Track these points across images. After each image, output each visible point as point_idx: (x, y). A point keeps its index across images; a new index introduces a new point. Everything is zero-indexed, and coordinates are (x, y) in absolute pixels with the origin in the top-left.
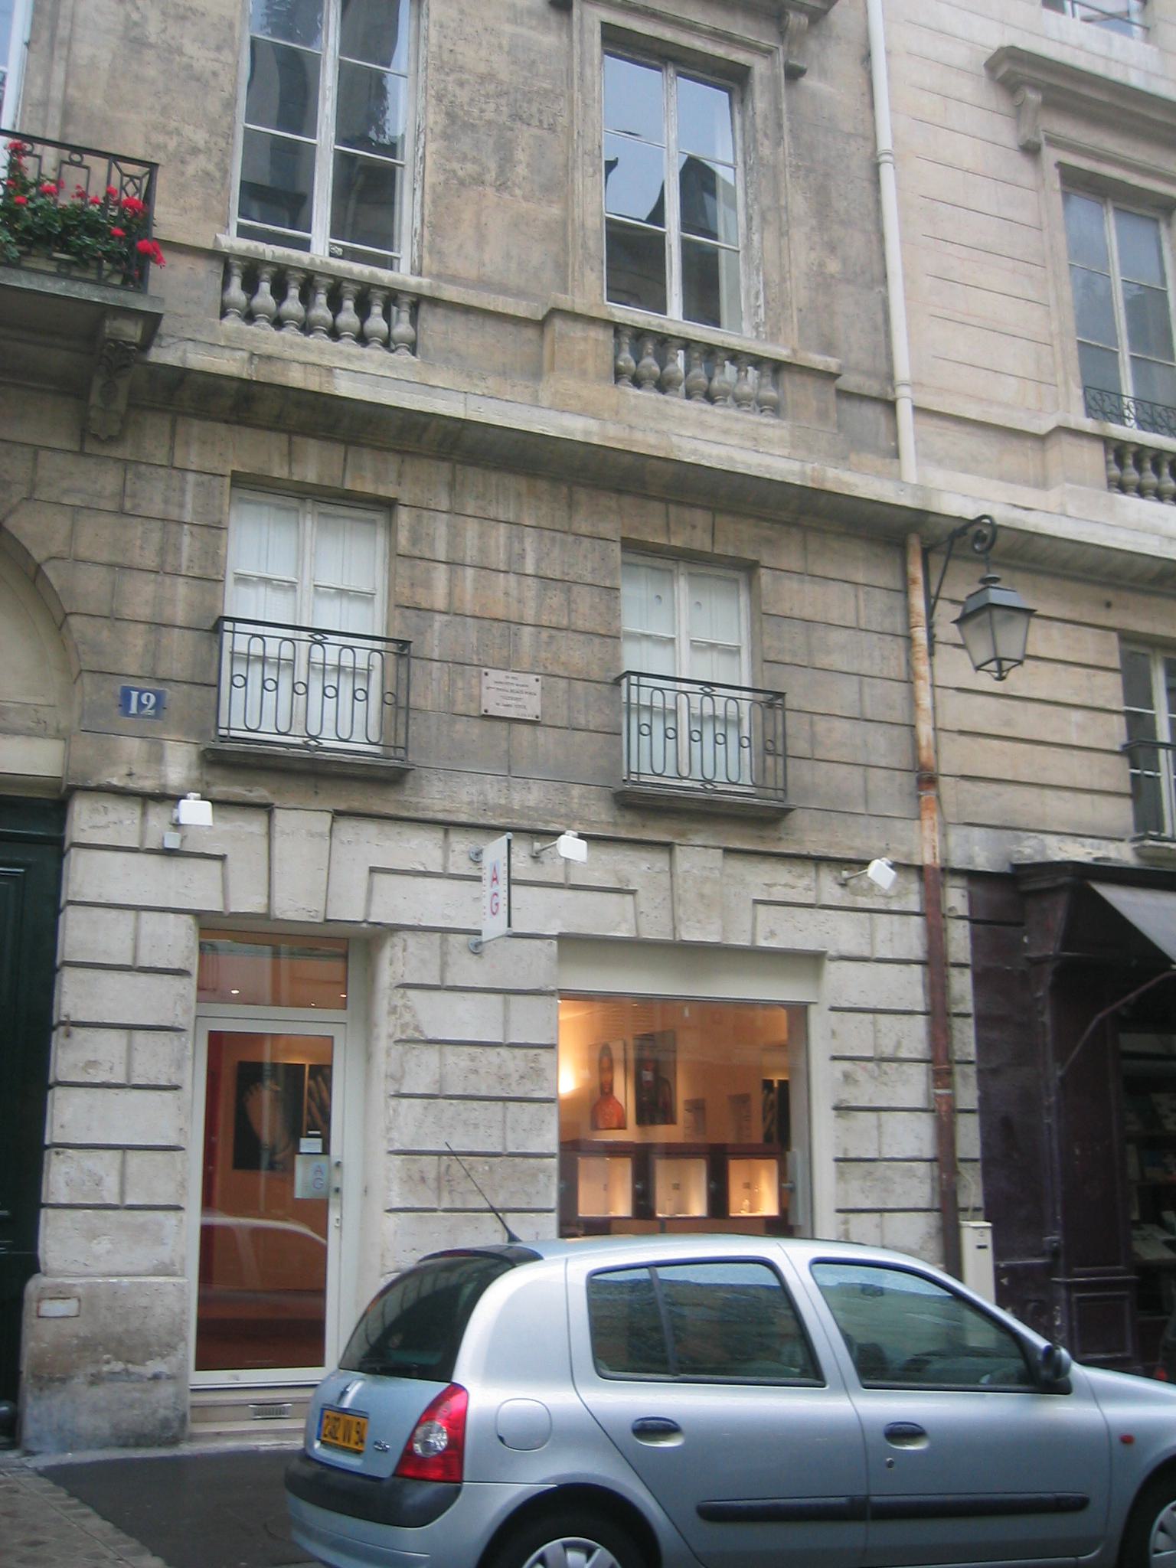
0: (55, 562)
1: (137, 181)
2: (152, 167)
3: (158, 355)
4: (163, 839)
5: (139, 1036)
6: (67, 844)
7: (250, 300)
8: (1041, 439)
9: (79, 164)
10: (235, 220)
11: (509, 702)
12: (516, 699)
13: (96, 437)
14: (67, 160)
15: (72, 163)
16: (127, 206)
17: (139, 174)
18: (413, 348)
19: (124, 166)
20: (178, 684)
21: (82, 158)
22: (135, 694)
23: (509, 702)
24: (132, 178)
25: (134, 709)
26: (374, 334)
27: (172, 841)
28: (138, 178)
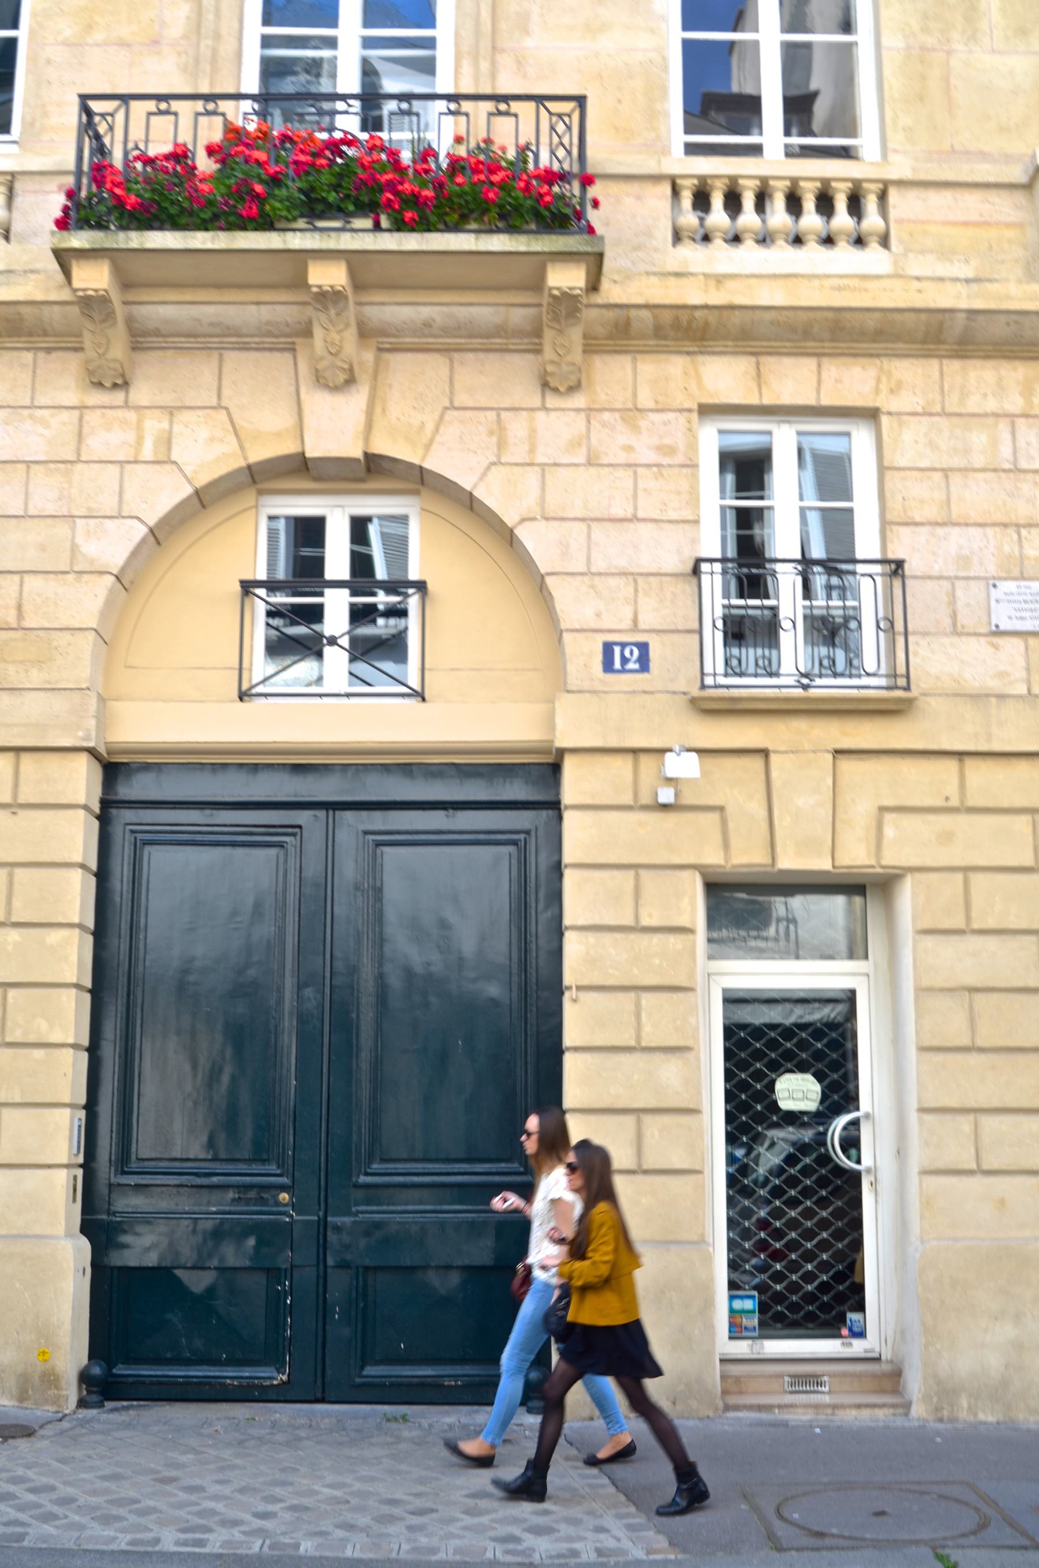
0: (527, 524)
1: (109, 118)
2: (581, 100)
3: (612, 292)
4: (656, 794)
5: (647, 1000)
6: (562, 807)
7: (702, 220)
8: (138, 518)
9: (507, 114)
10: (679, 138)
11: (1024, 614)
12: (1032, 610)
13: (556, 390)
14: (203, 111)
15: (500, 113)
16: (327, 148)
17: (110, 110)
18: (885, 241)
19: (555, 107)
20: (673, 627)
21: (508, 105)
22: (617, 650)
23: (1024, 614)
24: (560, 116)
25: (617, 665)
26: (840, 232)
27: (666, 795)
28: (565, 115)
